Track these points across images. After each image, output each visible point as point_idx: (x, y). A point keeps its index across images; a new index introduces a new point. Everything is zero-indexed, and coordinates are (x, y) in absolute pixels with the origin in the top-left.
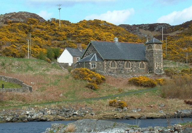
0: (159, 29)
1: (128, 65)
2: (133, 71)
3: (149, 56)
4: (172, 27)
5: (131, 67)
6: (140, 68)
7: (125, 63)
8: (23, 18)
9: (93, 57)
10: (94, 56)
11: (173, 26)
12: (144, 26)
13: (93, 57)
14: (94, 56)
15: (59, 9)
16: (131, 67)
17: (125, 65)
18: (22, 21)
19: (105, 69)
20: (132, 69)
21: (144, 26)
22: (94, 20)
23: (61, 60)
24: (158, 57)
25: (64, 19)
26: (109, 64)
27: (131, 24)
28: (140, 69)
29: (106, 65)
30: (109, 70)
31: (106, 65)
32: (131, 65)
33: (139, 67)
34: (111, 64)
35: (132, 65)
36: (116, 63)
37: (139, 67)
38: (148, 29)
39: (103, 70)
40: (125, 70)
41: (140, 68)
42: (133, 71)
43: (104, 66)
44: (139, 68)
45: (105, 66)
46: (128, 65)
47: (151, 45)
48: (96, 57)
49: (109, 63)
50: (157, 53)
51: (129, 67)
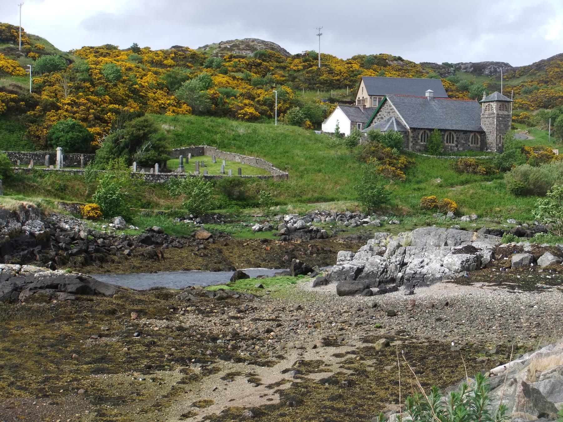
0: (491, 72)
1: (425, 138)
2: (458, 149)
3: (487, 123)
4: (514, 69)
5: (455, 143)
6: (472, 144)
7: (471, 137)
8: (252, 49)
9: (389, 123)
10: (391, 121)
11: (517, 68)
12: (463, 67)
13: (389, 123)
14: (391, 121)
15: (320, 35)
16: (455, 143)
17: (445, 138)
18: (252, 55)
19: (411, 144)
20: (457, 146)
21: (463, 67)
22: (380, 54)
23: (328, 126)
24: (502, 126)
25: (326, 53)
26: (417, 137)
27: (440, 63)
28: (471, 145)
29: (412, 137)
30: (417, 147)
31: (412, 137)
32: (455, 139)
33: (469, 142)
34: (422, 137)
35: (458, 138)
36: (455, 136)
37: (469, 142)
38: (471, 72)
39: (408, 147)
40: (445, 148)
41: (472, 144)
42: (458, 149)
43: (408, 139)
44: (470, 143)
45: (411, 139)
46: (425, 138)
47: (507, 104)
48: (395, 124)
49: (419, 134)
50: (501, 119)
51: (453, 143)
